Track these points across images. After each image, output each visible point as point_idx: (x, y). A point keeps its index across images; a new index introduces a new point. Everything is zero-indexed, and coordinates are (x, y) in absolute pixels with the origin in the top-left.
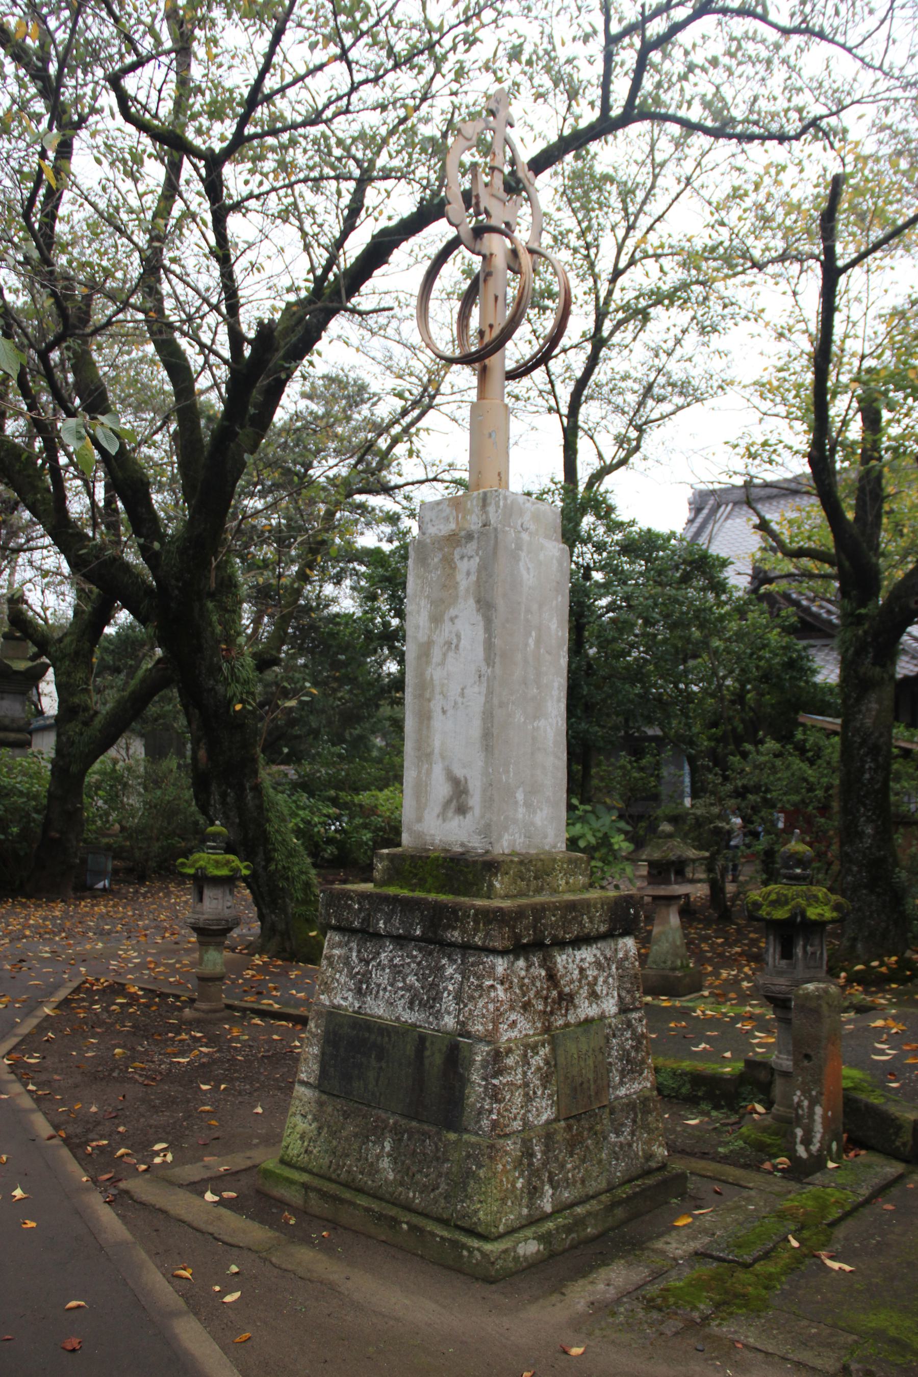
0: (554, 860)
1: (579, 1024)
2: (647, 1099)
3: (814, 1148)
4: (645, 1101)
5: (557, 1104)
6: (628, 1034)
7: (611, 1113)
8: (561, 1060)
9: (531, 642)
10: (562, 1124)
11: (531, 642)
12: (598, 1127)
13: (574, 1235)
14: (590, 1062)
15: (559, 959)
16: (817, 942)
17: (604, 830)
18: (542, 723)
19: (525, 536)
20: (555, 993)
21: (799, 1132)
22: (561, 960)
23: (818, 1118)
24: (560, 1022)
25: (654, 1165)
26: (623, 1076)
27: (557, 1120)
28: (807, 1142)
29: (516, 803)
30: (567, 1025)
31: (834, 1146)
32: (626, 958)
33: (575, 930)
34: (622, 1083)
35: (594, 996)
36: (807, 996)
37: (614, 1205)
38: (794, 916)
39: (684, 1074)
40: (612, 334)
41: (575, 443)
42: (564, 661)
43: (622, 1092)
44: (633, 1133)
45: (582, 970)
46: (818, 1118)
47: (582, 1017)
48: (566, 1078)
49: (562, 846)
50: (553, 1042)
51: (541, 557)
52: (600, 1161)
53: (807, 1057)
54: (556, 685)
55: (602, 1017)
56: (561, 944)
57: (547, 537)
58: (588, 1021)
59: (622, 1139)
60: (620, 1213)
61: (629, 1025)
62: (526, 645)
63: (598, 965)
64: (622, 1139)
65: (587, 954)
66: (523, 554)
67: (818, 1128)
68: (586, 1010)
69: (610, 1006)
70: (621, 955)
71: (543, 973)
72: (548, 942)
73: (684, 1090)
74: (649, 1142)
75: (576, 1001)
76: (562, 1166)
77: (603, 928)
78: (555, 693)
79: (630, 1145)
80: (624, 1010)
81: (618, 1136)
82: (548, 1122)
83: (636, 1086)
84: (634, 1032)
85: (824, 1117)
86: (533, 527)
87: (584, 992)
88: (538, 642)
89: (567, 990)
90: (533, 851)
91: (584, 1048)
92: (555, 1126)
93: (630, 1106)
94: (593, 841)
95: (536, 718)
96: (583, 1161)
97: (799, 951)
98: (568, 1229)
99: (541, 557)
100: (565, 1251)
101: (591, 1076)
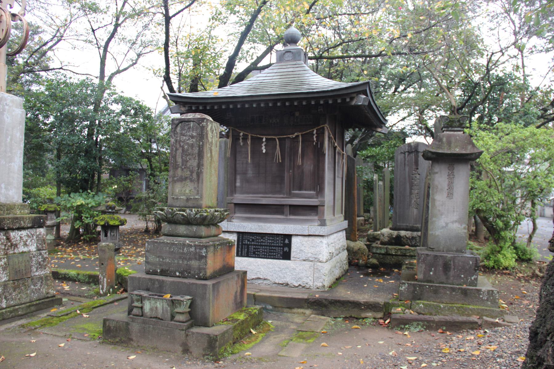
0: (15, 205)
1: (20, 253)
2: (47, 276)
3: (104, 290)
4: (46, 277)
5: (9, 276)
6: (40, 257)
7: (32, 280)
8: (11, 263)
9: (9, 140)
10: (11, 282)
11: (9, 140)
12: (26, 284)
13: (13, 314)
14: (24, 264)
15: (11, 234)
16: (115, 231)
17: (99, 201)
18: (13, 164)
19: (7, 107)
20: (9, 244)
21: (101, 286)
22: (12, 234)
23: (105, 282)
24: (12, 252)
25: (49, 295)
26: (37, 269)
27: (9, 281)
28: (103, 289)
29: (1, 188)
30: (14, 253)
31: (111, 290)
32: (40, 234)
33: (18, 225)
34: (37, 271)
35: (25, 245)
36: (102, 247)
37: (30, 306)
38: (105, 223)
39: (86, 275)
40: (122, 22)
41: (105, 62)
42: (22, 145)
43: (37, 274)
44: (41, 286)
45: (21, 237)
46: (105, 282)
47: (21, 251)
48: (13, 268)
49: (21, 201)
50: (8, 258)
51: (14, 114)
52: (27, 293)
53: (102, 264)
54: (19, 153)
55: (29, 251)
56: (13, 230)
57: (16, 107)
58: (23, 252)
59: (36, 287)
60: (33, 308)
61: (41, 254)
62: (6, 140)
63: (28, 236)
64: (36, 287)
65: (24, 233)
66: (5, 113)
67: (105, 285)
68: (22, 249)
69: (33, 248)
70: (38, 233)
71: (5, 238)
72: (6, 228)
73: (86, 280)
74: (48, 289)
75: (18, 246)
76: (10, 294)
77: (29, 225)
78: (18, 155)
79: (40, 289)
80: (39, 250)
81: (35, 286)
82: (5, 281)
83: (43, 272)
84: (43, 257)
85: (107, 281)
86: (11, 104)
87: (22, 243)
88: (11, 140)
89: (14, 243)
90: (8, 202)
91: (21, 260)
92: (8, 282)
93: (41, 278)
94: (94, 205)
95: (10, 162)
96: (20, 293)
97: (109, 234)
98: (11, 312)
99: (14, 114)
100: (8, 319)
101: (24, 268)
